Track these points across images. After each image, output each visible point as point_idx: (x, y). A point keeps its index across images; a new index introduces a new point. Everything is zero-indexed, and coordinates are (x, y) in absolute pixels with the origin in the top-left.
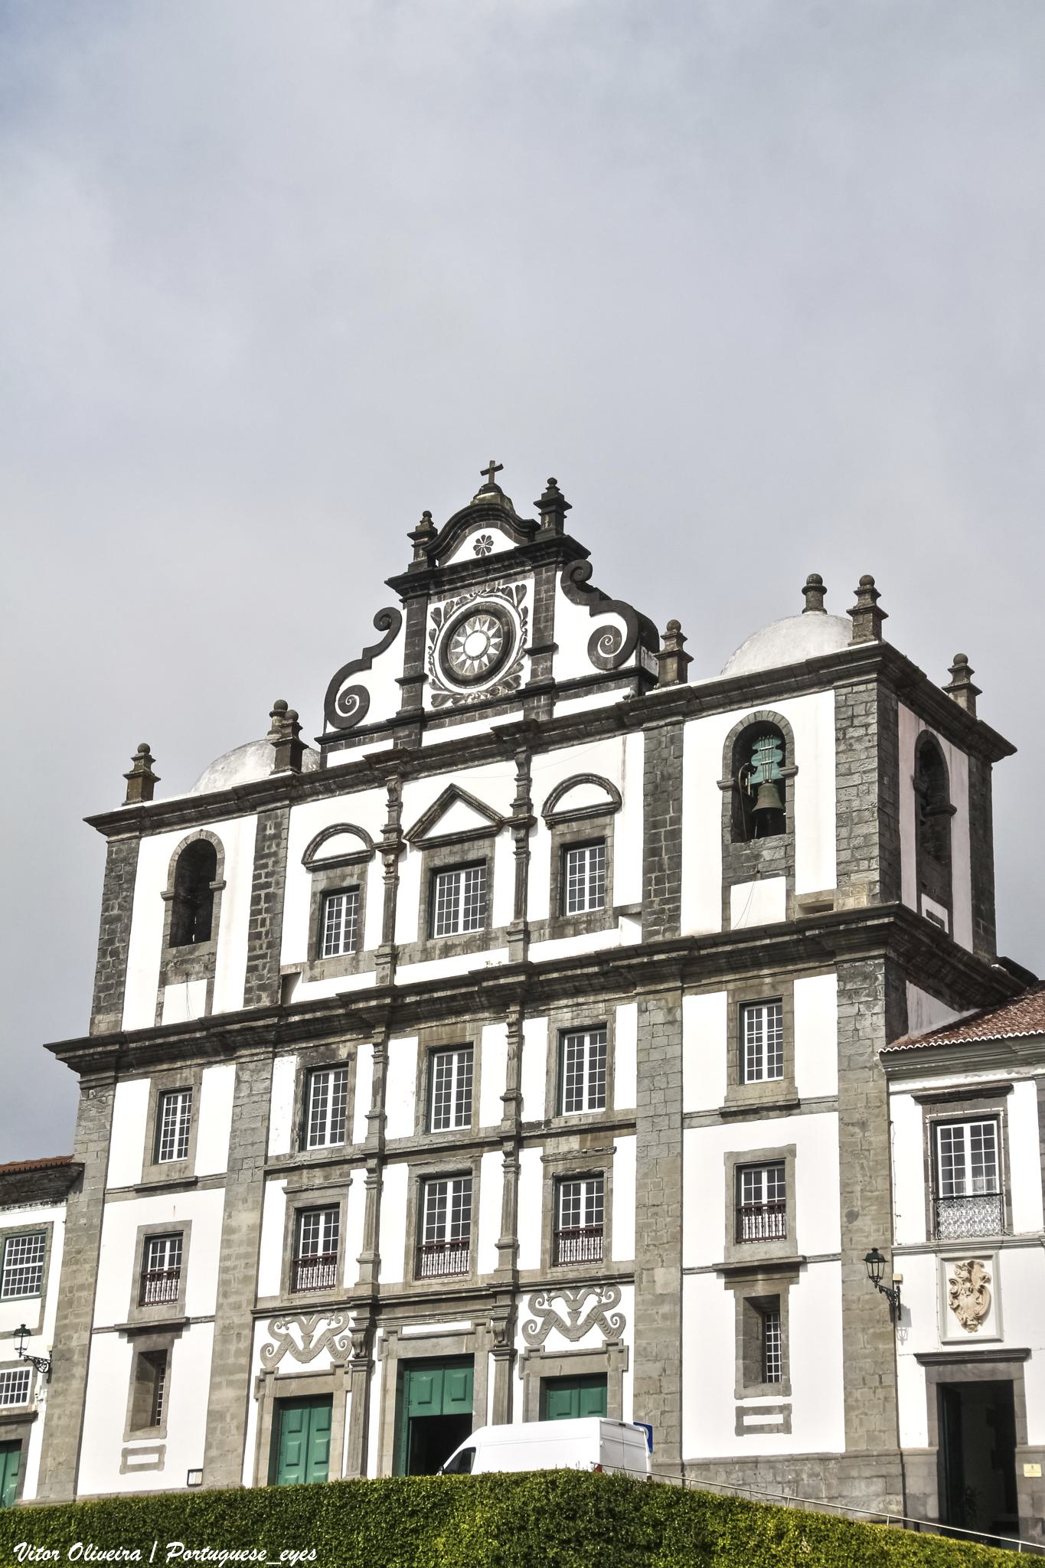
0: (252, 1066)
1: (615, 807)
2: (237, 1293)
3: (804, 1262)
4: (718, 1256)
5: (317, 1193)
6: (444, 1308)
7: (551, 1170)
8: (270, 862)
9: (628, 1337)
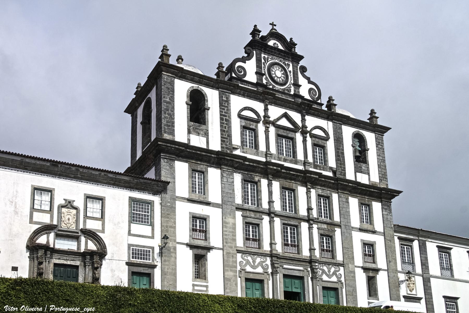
0: (227, 172)
1: (327, 139)
2: (230, 243)
3: (212, 248)
4: (187, 240)
5: (252, 219)
6: (295, 262)
7: (320, 232)
8: (226, 109)
9: (343, 279)
